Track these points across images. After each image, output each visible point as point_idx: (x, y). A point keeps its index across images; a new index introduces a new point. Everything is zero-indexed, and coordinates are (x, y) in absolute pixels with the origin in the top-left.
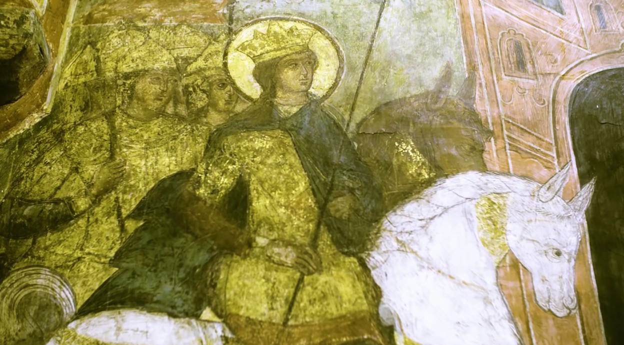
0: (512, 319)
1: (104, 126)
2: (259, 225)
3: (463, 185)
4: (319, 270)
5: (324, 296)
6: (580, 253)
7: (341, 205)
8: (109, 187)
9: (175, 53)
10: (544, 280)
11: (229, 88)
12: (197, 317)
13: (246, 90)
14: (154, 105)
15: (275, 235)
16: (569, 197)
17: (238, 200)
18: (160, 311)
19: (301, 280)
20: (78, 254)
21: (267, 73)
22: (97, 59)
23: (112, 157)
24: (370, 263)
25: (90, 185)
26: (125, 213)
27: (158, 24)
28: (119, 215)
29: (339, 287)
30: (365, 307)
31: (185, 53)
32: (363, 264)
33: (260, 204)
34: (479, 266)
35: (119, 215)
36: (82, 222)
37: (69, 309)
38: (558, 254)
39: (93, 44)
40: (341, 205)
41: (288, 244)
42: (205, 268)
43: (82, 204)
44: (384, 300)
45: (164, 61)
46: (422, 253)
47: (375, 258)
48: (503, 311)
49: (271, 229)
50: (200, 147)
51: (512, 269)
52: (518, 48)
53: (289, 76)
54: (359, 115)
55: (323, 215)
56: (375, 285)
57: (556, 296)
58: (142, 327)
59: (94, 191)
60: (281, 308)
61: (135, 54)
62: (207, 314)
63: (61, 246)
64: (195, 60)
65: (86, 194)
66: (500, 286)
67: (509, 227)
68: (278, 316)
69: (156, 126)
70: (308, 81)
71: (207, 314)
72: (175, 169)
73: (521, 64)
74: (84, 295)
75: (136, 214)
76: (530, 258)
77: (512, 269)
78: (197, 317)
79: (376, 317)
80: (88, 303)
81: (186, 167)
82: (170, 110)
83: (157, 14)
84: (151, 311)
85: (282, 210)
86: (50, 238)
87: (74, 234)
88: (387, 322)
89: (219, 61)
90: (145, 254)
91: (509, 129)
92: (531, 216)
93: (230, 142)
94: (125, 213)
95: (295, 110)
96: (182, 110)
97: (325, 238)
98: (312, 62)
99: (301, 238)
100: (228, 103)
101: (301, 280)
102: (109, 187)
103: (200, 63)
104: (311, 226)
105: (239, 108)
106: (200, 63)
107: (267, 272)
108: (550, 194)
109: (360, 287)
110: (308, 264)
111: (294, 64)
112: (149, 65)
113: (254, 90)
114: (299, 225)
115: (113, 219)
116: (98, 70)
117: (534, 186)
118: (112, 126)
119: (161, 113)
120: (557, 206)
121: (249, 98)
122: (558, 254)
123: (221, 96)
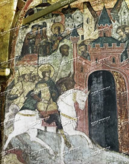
0: (76, 111)
1: (21, 83)
2: (43, 98)
3: (71, 91)
4: (51, 104)
5: (51, 107)
6: (86, 101)
7: (53, 95)
8: (22, 93)
9: (30, 71)
10: (81, 105)
11: (38, 77)
12: (35, 110)
13: (41, 77)
14: (28, 80)
15: (45, 99)
16: (86, 93)
17: (40, 94)
18: (30, 110)
19: (48, 105)
20: (19, 102)
21: (44, 74)
22: (19, 72)
23: (22, 88)
24: (57, 103)
25: (20, 92)
26: (25, 96)
27: (27, 65)
28: (24, 97)
29: (52, 107)
30: (56, 109)
31: (32, 70)
32: (56, 103)
33: (43, 95)
34: (72, 103)
35: (24, 97)
36: (19, 98)
37: (19, 110)
38: (83, 101)
39: (18, 69)
40: (53, 95)
41: (46, 100)
42: (36, 104)
43: (19, 95)
44: (59, 107)
45: (28, 72)
46: (64, 101)
47: (58, 102)
48: (74, 109)
49: (44, 98)
50: (35, 85)
51: (76, 104)
52: (82, 68)
53: (47, 74)
54: (57, 80)
55: (51, 96)
56: (58, 106)
57: (82, 107)
58: (28, 112)
59: (20, 93)
60: (45, 109)
61: (24, 71)
62: (36, 110)
63: (16, 101)
64: (33, 72)
65: (7, 87)
66: (75, 106)
67: (77, 97)
68: (45, 110)
69: (28, 83)
70: (49, 75)
71: (36, 110)
72: (31, 90)
73: (82, 71)
74: (20, 108)
75: (26, 96)
76: (79, 102)
77: (76, 104)
78: (35, 110)
79: (58, 110)
80: (21, 109)
81: (33, 89)
82: (30, 81)
83: (27, 64)
84: (29, 110)
85: (46, 96)
86: (15, 100)
87: (18, 99)
88: (59, 111)
89: (37, 72)
90: (28, 102)
91: (79, 82)
92: (80, 96)
93: (38, 86)
94: (25, 96)
95: (48, 80)
96: (32, 80)
97: (51, 100)
98: (50, 71)
99: (48, 100)
100: (38, 79)
101: (48, 105)
102: (22, 93)
103: (34, 72)
104: (50, 98)
105: (40, 80)
106: (34, 72)
107: (55, 108)
108: (83, 93)
109: (56, 106)
110: (49, 103)
111: (48, 72)
112: (26, 73)
113: (42, 77)
114: (48, 98)
115: (23, 97)
116: (19, 74)
117: (81, 91)
118: (22, 83)
119: (29, 81)
120: (84, 94)
121: (41, 78)
122: (83, 101)
123: (37, 78)
